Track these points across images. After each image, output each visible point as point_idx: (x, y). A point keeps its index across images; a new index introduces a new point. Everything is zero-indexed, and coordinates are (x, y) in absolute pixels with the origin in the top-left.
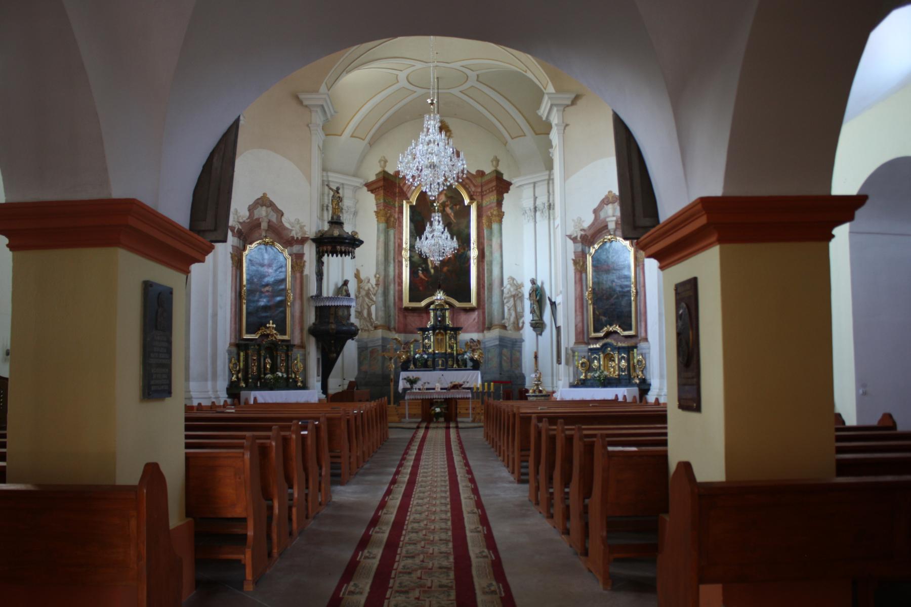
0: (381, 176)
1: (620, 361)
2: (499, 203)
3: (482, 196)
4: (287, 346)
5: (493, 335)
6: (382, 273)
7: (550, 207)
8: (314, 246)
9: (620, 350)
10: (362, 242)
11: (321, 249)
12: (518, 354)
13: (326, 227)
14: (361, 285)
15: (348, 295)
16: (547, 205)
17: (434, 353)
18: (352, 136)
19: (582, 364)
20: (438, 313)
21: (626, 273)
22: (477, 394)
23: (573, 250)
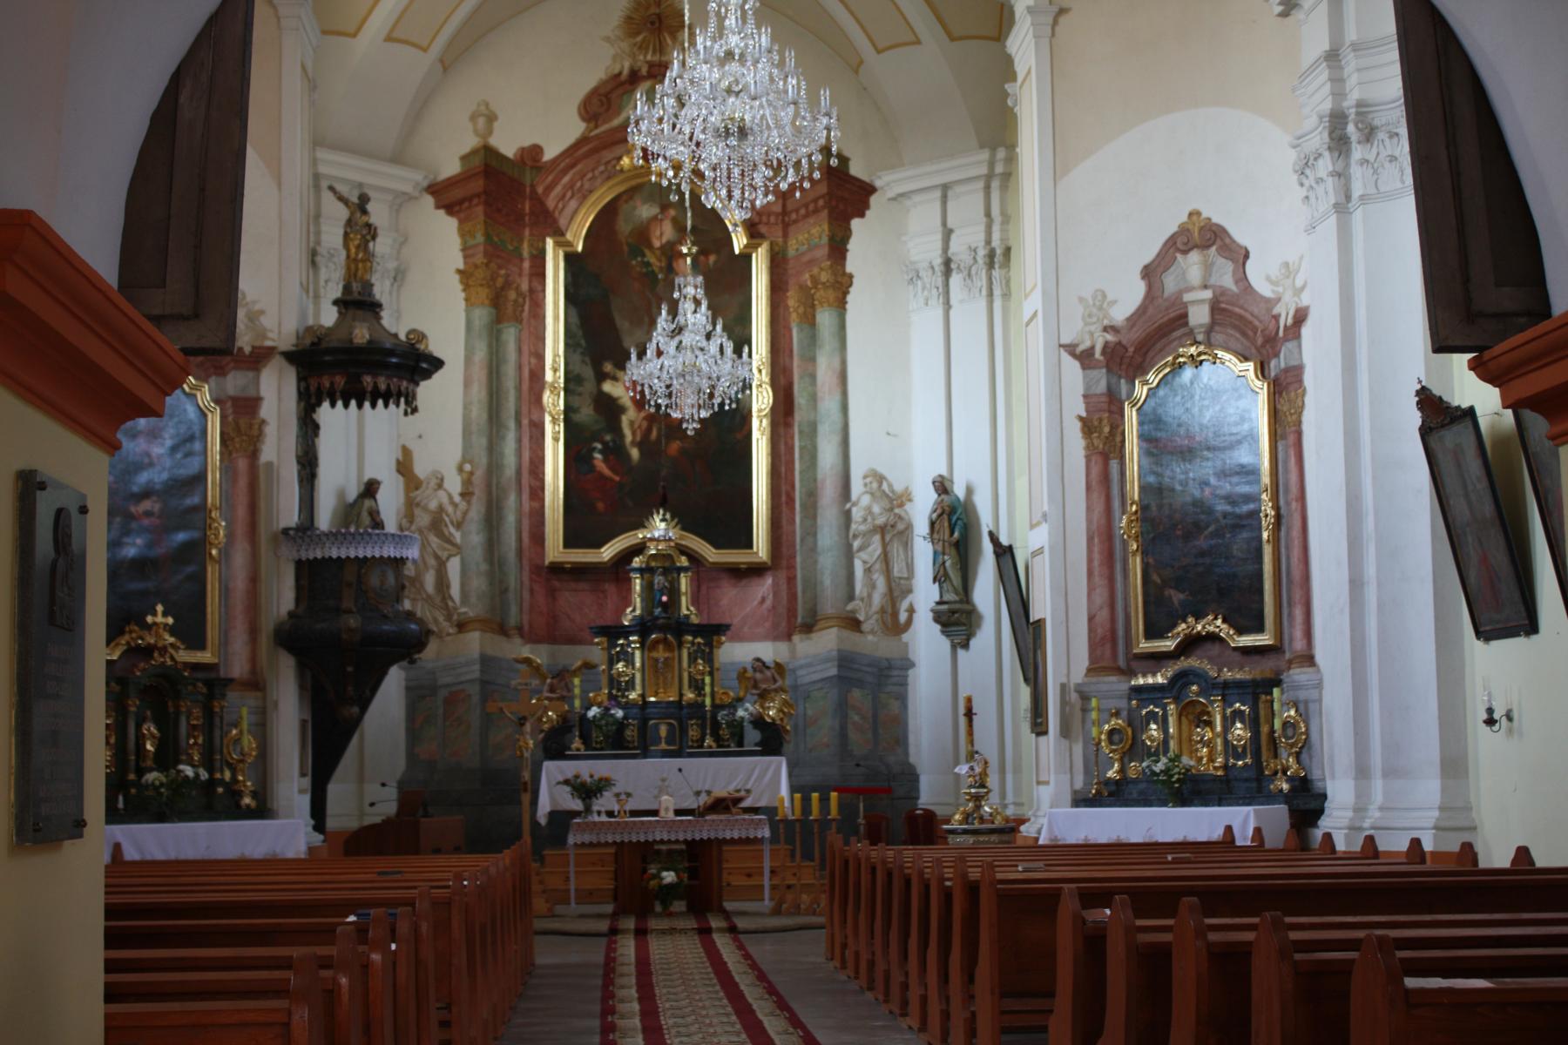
0: (477, 161)
1: (1228, 724)
2: (838, 249)
3: (786, 227)
4: (210, 684)
5: (816, 650)
6: (483, 460)
7: (998, 258)
8: (291, 376)
9: (1228, 690)
10: (438, 364)
11: (313, 383)
12: (895, 706)
13: (329, 317)
14: (418, 495)
15: (378, 524)
16: (982, 252)
17: (646, 704)
18: (389, 39)
19: (1111, 732)
20: (659, 580)
21: (1243, 456)
22: (795, 835)
23: (1081, 390)
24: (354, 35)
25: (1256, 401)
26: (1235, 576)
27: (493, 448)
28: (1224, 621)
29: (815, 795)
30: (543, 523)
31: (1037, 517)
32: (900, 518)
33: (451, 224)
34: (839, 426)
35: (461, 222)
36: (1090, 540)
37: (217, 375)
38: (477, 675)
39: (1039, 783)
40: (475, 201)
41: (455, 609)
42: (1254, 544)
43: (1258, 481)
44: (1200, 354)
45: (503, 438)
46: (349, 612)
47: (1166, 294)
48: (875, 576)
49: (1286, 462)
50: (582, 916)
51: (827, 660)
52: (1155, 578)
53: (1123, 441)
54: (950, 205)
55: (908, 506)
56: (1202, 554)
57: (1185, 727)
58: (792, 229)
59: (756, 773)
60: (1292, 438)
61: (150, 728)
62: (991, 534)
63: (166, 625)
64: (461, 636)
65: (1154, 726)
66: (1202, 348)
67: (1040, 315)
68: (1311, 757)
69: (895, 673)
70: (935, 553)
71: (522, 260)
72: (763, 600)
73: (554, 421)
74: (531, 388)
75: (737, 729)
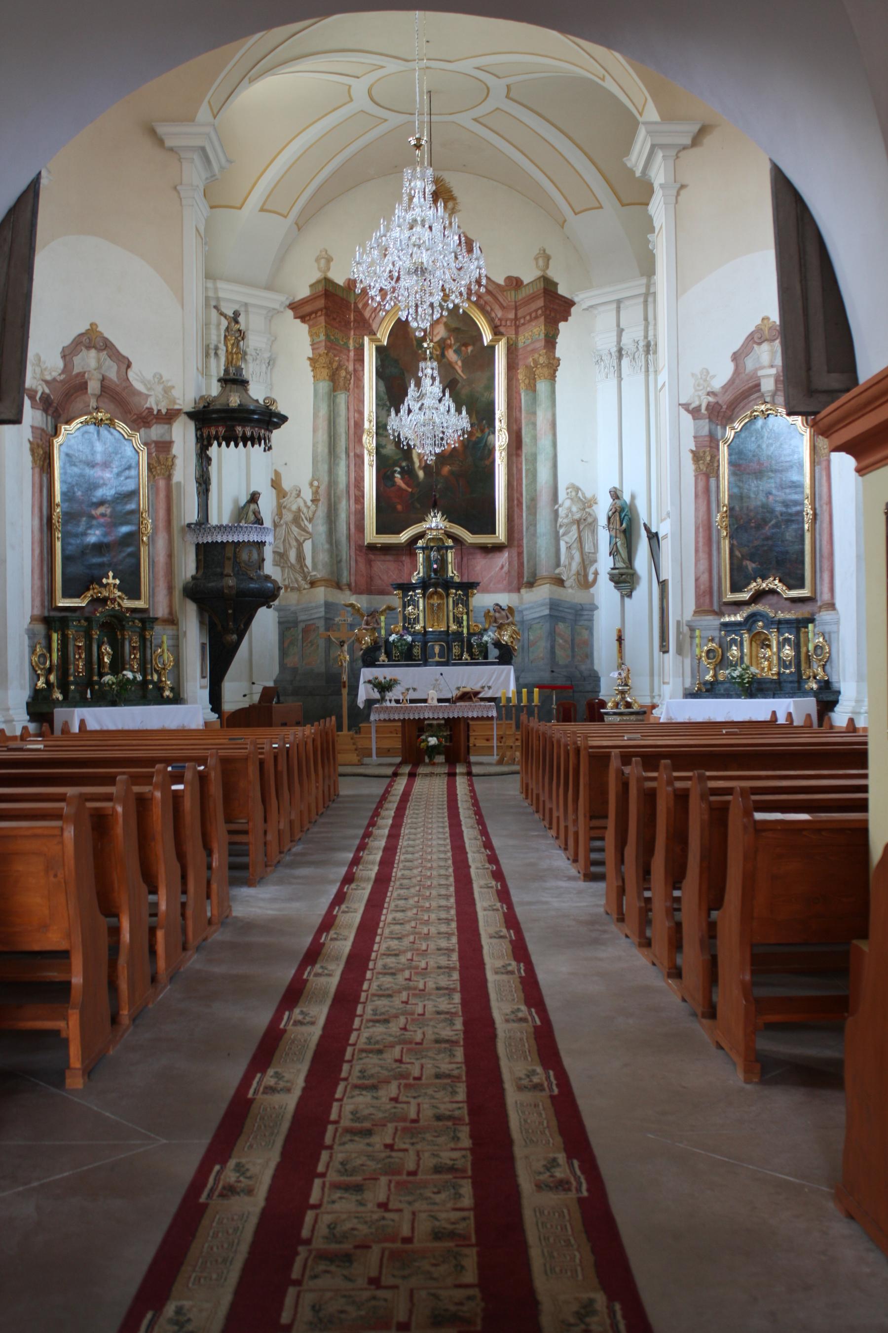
0: (320, 288)
1: (780, 646)
2: (551, 342)
3: (517, 327)
4: (143, 621)
7: (649, 348)
8: (191, 426)
9: (780, 625)
11: (205, 432)
12: (585, 634)
13: (215, 390)
14: (285, 501)
16: (642, 344)
18: (262, 210)
19: (708, 652)
20: (433, 554)
23: (693, 434)
24: (240, 208)
25: (802, 440)
26: (787, 552)
27: (331, 471)
28: (780, 581)
29: (525, 690)
30: (363, 519)
31: (664, 515)
32: (590, 514)
33: (305, 327)
34: (551, 456)
35: (310, 327)
36: (697, 529)
37: (145, 427)
38: (323, 614)
39: (664, 683)
40: (319, 313)
41: (309, 573)
42: (800, 532)
43: (803, 492)
44: (767, 410)
45: (338, 465)
46: (229, 576)
47: (747, 371)
48: (573, 552)
49: (820, 479)
50: (380, 765)
51: (542, 605)
52: (737, 553)
53: (718, 466)
54: (622, 312)
55: (595, 507)
56: (767, 539)
57: (754, 649)
58: (521, 329)
59: (494, 677)
60: (824, 464)
61: (107, 648)
62: (645, 525)
63: (115, 585)
64: (312, 590)
65: (734, 648)
66: (769, 406)
67: (667, 384)
68: (831, 668)
69: (585, 613)
70: (611, 537)
71: (349, 351)
72: (502, 567)
73: (370, 453)
74: (355, 433)
75: (484, 651)
